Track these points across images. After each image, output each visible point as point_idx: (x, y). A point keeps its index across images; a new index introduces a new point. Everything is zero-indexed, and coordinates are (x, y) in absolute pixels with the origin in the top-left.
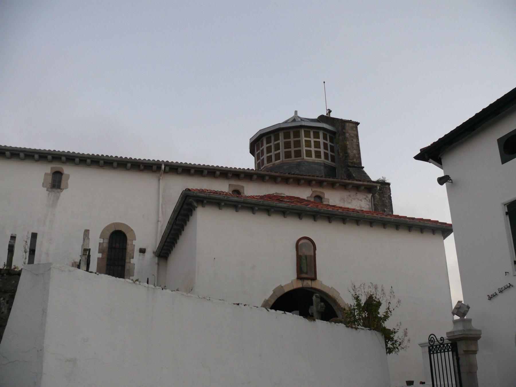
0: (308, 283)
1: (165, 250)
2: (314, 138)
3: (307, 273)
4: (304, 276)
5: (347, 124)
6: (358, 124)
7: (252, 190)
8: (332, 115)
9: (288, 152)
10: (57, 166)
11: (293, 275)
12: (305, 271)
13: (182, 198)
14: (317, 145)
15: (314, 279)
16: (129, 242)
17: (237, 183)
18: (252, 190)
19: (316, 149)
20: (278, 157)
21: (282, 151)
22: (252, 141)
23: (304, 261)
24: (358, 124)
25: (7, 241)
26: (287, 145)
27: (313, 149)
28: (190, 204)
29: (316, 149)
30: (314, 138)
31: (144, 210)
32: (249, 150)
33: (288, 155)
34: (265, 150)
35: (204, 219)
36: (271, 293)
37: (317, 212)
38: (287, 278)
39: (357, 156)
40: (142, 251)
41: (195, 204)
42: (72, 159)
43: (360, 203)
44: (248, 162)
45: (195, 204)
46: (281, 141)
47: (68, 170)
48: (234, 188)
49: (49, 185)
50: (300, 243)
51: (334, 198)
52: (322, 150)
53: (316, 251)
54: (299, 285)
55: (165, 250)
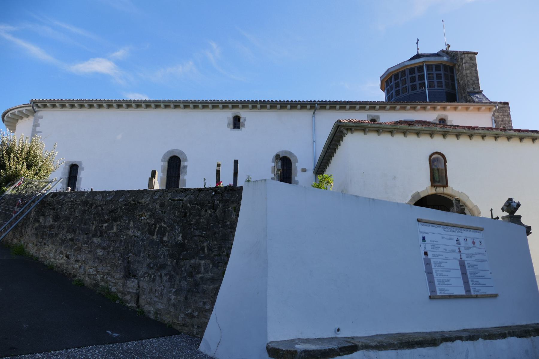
0: (440, 190)
1: (321, 167)
2: (437, 79)
3: (439, 182)
4: (437, 184)
5: (466, 55)
6: (476, 53)
7: (387, 117)
8: (451, 49)
9: (414, 85)
10: (438, 144)
11: (428, 183)
12: (438, 180)
13: (335, 128)
14: (439, 76)
15: (446, 185)
16: (292, 164)
17: (373, 113)
18: (387, 117)
19: (438, 80)
20: (405, 90)
21: (409, 84)
22: (382, 79)
23: (436, 172)
24: (476, 53)
25: (215, 168)
26: (413, 79)
27: (435, 80)
28: (342, 132)
29: (438, 80)
30: (437, 79)
31: (303, 139)
32: (380, 87)
33: (414, 88)
34: (394, 86)
35: (351, 142)
36: (410, 198)
37: (442, 128)
38: (423, 186)
39: (476, 82)
40: (304, 170)
41: (345, 131)
42: (245, 105)
43: (483, 119)
44: (381, 96)
45: (345, 131)
46: (408, 77)
47: (244, 114)
48: (371, 118)
49: (232, 126)
50: (433, 157)
51: (458, 116)
52: (443, 80)
53: (447, 164)
54: (433, 191)
55: (321, 167)
